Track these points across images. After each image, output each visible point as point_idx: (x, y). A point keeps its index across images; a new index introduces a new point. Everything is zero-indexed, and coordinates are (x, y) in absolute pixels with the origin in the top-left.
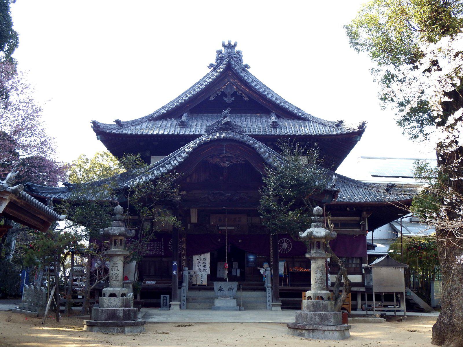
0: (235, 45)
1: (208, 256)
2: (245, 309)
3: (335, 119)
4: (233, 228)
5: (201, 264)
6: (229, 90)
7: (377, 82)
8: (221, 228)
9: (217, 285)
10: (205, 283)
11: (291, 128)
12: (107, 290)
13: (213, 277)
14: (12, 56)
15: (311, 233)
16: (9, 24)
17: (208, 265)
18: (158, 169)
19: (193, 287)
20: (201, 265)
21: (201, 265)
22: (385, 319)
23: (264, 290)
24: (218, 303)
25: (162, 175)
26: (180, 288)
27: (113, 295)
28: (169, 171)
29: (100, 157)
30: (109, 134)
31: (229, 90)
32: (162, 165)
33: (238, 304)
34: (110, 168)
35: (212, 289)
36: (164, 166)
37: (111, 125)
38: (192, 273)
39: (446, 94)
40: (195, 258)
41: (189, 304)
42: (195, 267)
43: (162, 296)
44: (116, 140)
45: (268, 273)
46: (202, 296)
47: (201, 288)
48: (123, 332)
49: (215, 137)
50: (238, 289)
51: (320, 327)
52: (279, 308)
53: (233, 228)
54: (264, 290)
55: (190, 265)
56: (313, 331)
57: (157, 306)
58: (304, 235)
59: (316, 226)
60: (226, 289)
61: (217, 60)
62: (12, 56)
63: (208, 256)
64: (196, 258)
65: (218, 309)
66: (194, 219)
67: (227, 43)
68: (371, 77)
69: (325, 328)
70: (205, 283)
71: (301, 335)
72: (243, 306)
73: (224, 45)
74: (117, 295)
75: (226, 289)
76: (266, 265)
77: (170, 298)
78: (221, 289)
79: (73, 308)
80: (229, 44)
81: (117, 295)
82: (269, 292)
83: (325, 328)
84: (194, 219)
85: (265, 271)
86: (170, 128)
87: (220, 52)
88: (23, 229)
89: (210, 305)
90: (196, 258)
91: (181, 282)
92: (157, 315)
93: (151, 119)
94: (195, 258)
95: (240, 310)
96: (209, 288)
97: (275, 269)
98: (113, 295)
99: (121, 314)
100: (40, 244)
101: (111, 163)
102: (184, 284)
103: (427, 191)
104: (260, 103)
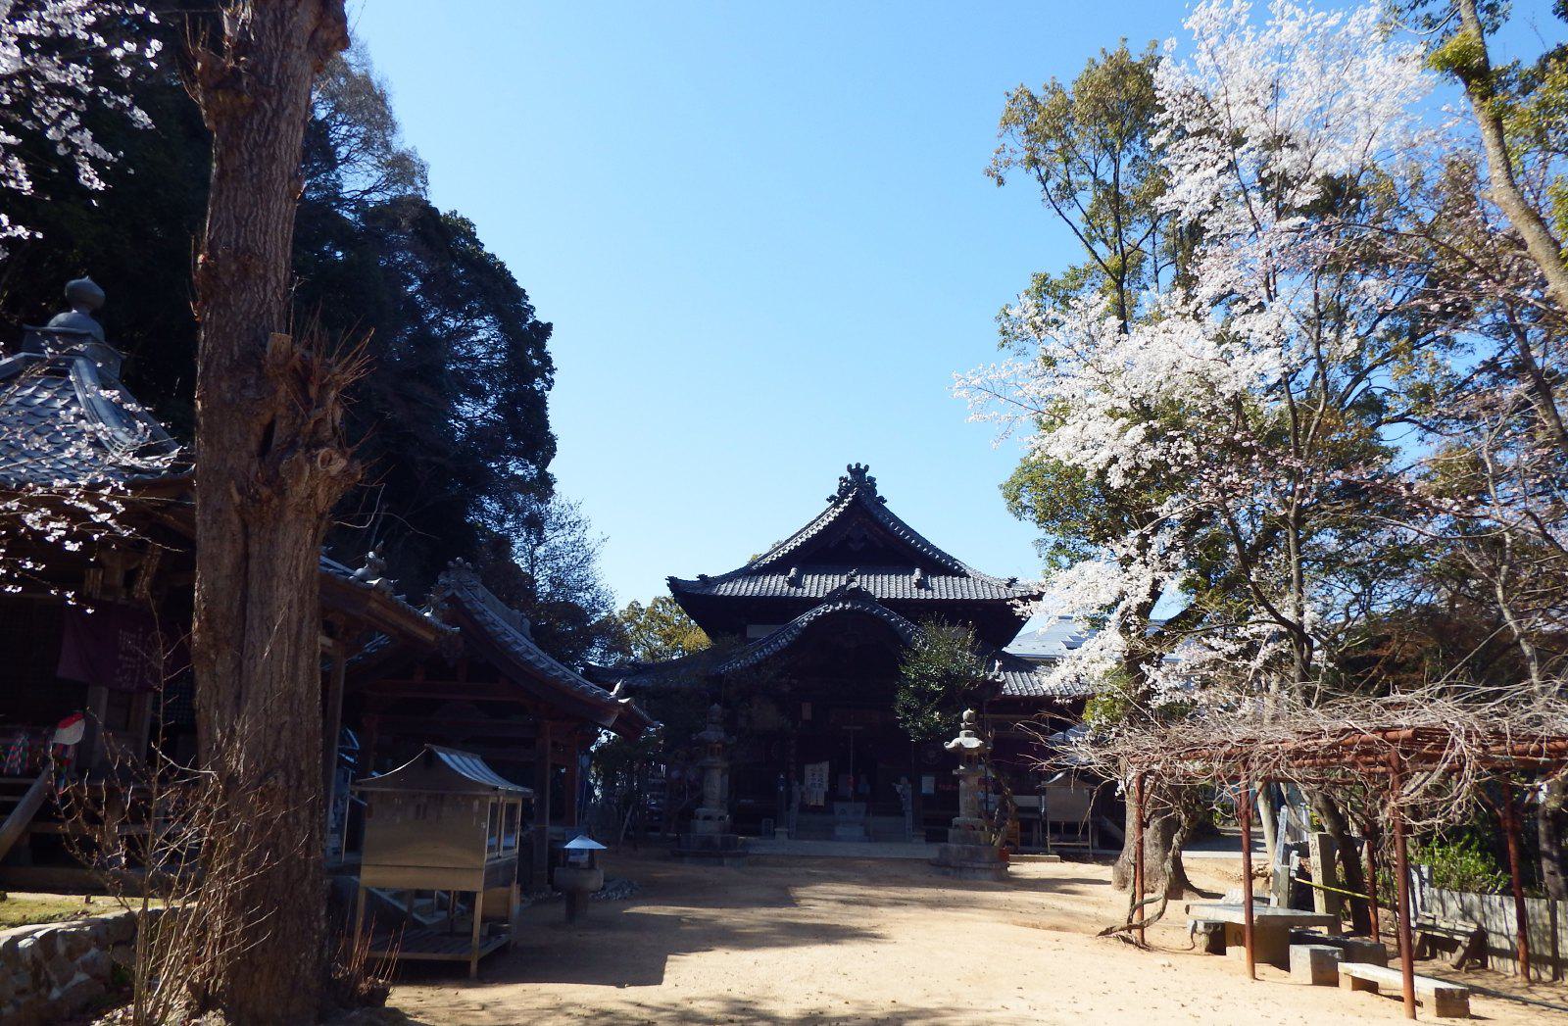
0: (867, 468)
2: (876, 841)
3: (1007, 576)
4: (861, 728)
5: (816, 777)
6: (861, 528)
7: (1043, 557)
8: (844, 727)
9: (838, 806)
10: (821, 803)
11: (943, 588)
12: (702, 811)
13: (833, 795)
14: (549, 470)
15: (960, 745)
16: (546, 425)
17: (826, 778)
18: (762, 650)
19: (804, 808)
20: (817, 778)
21: (817, 778)
23: (902, 814)
24: (839, 831)
25: (767, 660)
26: (788, 809)
27: (707, 818)
28: (777, 654)
29: (660, 605)
31: (861, 528)
32: (767, 640)
33: (867, 833)
34: (273, 158)
35: (832, 812)
36: (768, 646)
37: (900, 913)
38: (804, 789)
42: (808, 781)
43: (764, 821)
44: (693, 597)
45: (909, 792)
47: (816, 809)
48: (721, 864)
49: (837, 608)
50: (867, 812)
51: (969, 864)
52: (923, 840)
53: (861, 728)
54: (902, 814)
55: (801, 779)
56: (961, 869)
57: (757, 833)
58: (951, 745)
59: (967, 735)
61: (839, 490)
62: (549, 470)
63: (825, 766)
64: (809, 769)
65: (839, 839)
66: (807, 713)
67: (854, 467)
68: (1034, 552)
69: (976, 865)
70: (821, 803)
71: (947, 874)
72: (872, 836)
74: (712, 819)
76: (904, 780)
77: (775, 822)
79: (651, 833)
80: (858, 465)
81: (712, 819)
83: (976, 865)
84: (807, 713)
85: (902, 787)
86: (776, 585)
89: (828, 833)
90: (809, 769)
91: (789, 802)
92: (760, 847)
93: (748, 572)
95: (870, 841)
96: (826, 809)
97: (917, 785)
98: (707, 818)
99: (719, 842)
101: (698, 638)
102: (793, 805)
104: (904, 550)
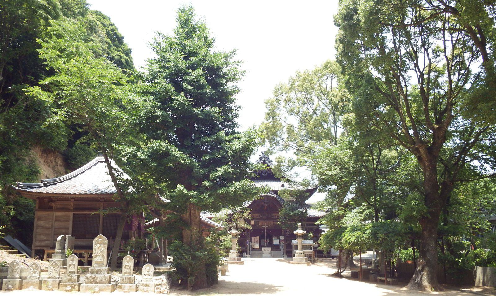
1: (258, 237)
19: (253, 250)
22: (40, 88)
24: (264, 255)
30: (335, 274)
33: (271, 256)
39: (86, 262)
40: (253, 238)
41: (252, 256)
47: (257, 250)
50: (271, 250)
60: (266, 250)
72: (273, 256)
73: (262, 153)
75: (266, 250)
78: (265, 250)
82: (282, 251)
87: (260, 155)
88: (452, 41)
89: (261, 256)
94: (253, 238)
103: (27, 206)
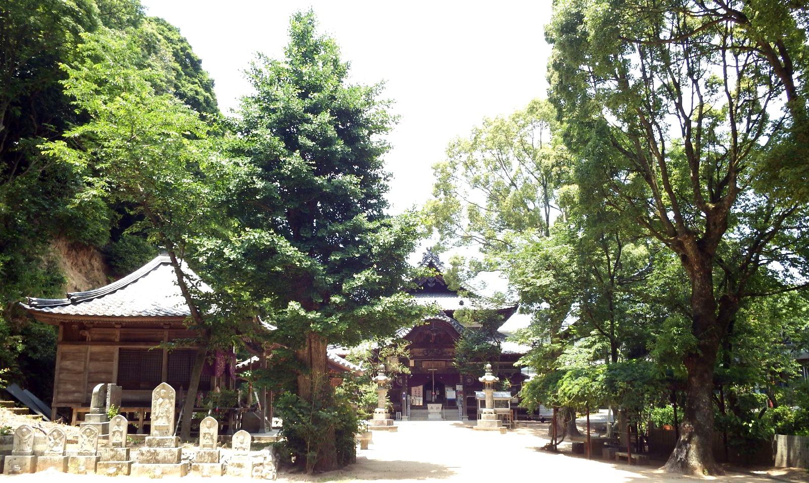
1: (421, 387)
19: (413, 407)
23: (457, 408)
24: (430, 416)
33: (442, 417)
39: (139, 427)
41: (412, 418)
46: (419, 413)
47: (419, 407)
50: (442, 408)
54: (457, 408)
60: (435, 408)
72: (445, 418)
73: (427, 249)
78: (432, 408)
82: (460, 409)
88: (737, 67)
89: (425, 417)
94: (413, 389)
100: (133, 256)
